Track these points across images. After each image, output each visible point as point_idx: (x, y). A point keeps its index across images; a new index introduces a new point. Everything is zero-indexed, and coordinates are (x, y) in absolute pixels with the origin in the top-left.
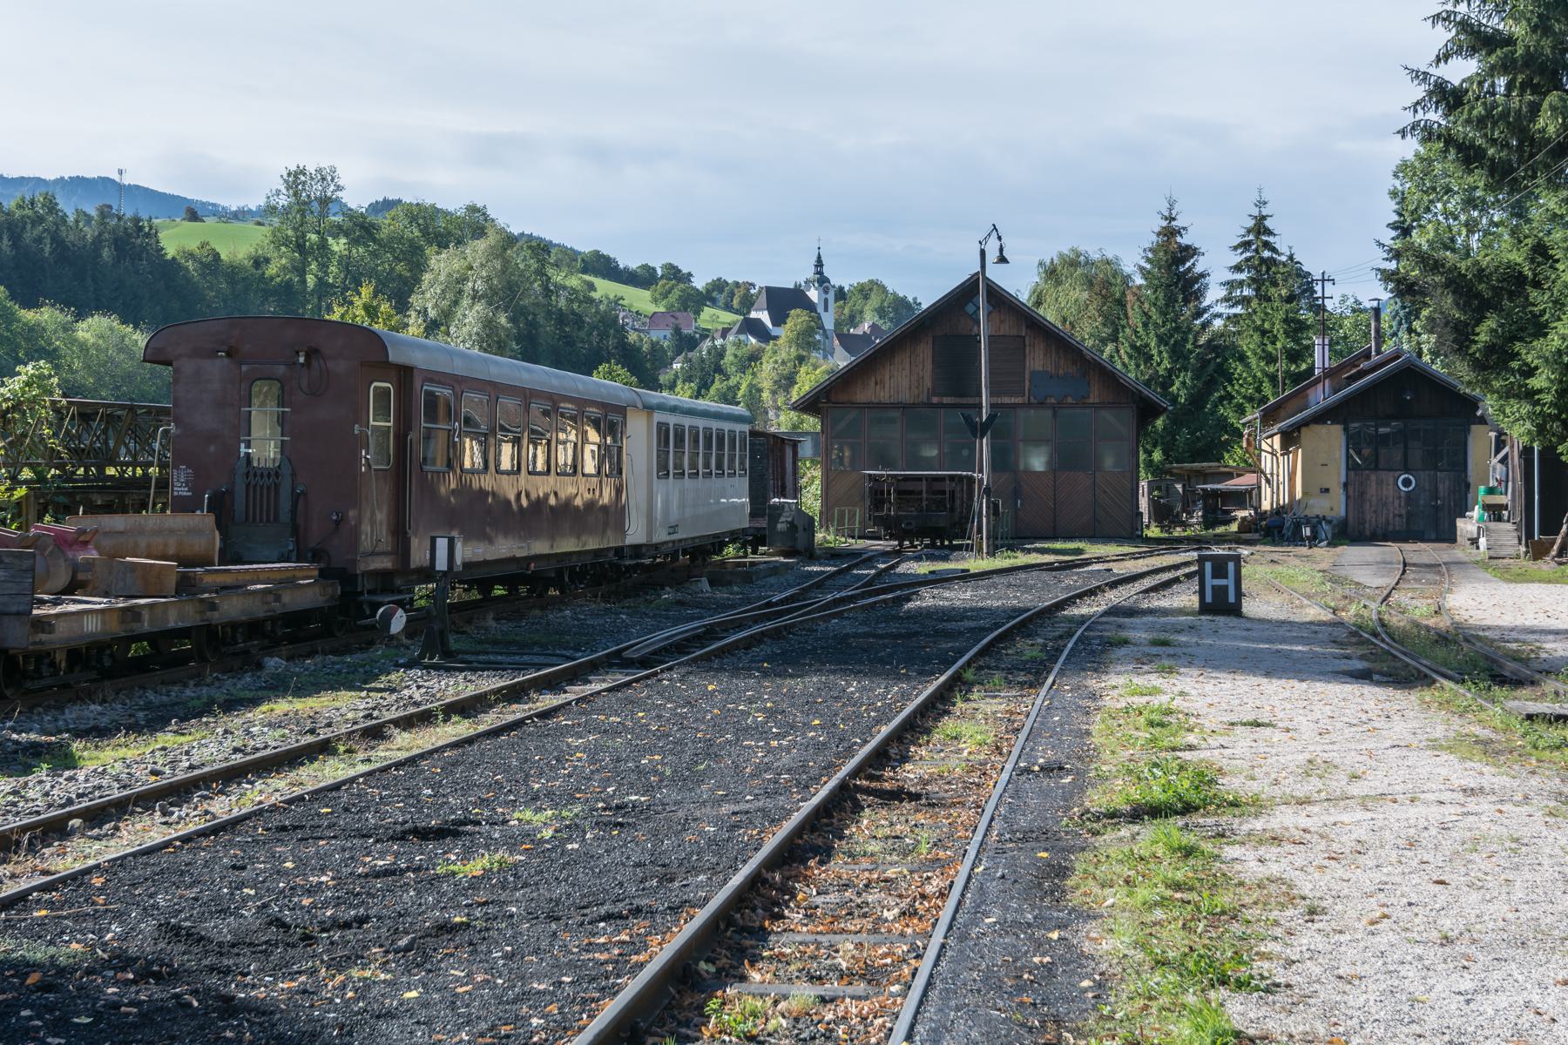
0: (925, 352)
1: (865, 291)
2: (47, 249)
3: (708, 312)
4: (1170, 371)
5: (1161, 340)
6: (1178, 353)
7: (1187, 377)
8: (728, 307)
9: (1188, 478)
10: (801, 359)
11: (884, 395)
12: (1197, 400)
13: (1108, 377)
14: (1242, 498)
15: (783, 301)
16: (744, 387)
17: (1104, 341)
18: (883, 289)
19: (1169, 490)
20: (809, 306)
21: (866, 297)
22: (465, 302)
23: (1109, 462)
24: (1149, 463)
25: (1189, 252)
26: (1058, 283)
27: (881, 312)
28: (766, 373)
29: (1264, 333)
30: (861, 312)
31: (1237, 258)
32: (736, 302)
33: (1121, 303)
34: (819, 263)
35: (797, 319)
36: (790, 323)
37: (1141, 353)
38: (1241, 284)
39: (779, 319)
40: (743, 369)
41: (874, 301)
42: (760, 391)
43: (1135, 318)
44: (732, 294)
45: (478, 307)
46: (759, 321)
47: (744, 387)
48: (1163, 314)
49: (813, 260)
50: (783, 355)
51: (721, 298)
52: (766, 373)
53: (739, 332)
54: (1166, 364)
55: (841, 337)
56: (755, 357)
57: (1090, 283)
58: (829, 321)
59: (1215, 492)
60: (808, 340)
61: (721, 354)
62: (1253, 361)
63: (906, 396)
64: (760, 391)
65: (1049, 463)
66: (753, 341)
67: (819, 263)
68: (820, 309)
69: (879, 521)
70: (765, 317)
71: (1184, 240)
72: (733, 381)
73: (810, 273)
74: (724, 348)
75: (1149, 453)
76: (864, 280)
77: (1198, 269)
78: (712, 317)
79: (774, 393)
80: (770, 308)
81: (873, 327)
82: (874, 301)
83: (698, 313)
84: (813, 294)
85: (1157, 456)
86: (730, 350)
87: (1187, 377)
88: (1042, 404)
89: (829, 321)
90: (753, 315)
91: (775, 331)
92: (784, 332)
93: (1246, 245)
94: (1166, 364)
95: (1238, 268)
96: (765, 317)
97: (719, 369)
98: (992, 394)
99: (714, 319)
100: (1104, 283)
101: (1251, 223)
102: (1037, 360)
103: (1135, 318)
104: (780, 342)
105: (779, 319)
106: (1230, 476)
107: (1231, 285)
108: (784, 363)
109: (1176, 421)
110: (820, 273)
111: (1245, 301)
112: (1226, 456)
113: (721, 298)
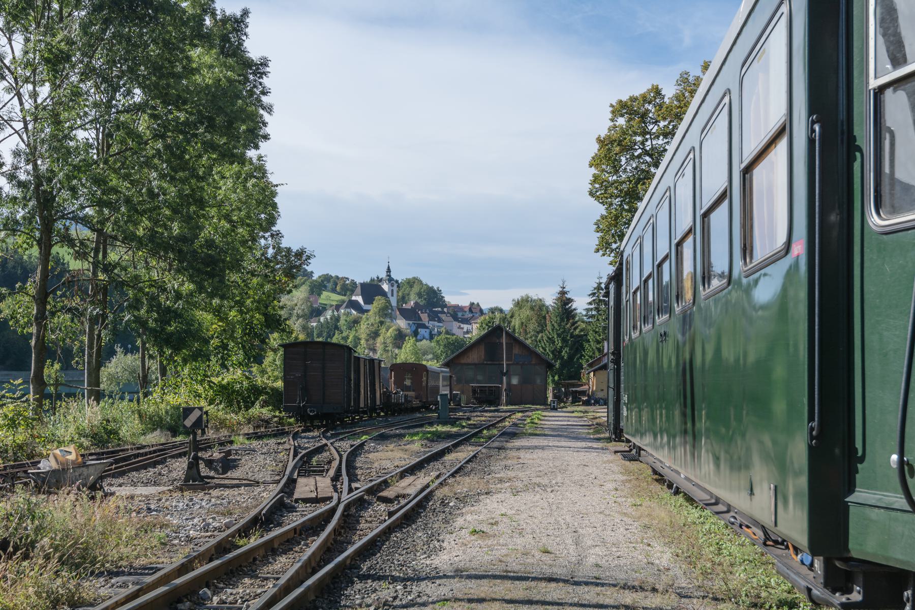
0: (482, 348)
1: (411, 283)
2: (19, 272)
3: (325, 294)
4: (561, 347)
5: (559, 335)
6: (564, 340)
7: (567, 349)
8: (334, 291)
9: (567, 386)
10: (382, 323)
11: (469, 361)
12: (571, 357)
13: (537, 355)
14: (583, 393)
15: (371, 290)
16: (351, 337)
17: (538, 333)
18: (420, 282)
19: (560, 390)
20: (384, 294)
21: (411, 287)
22: (294, 318)
23: (538, 381)
24: (553, 381)
25: (570, 301)
26: (520, 308)
27: (420, 295)
28: (363, 329)
29: (596, 332)
30: (408, 295)
31: (590, 299)
32: (338, 288)
33: (545, 318)
34: (389, 270)
35: (379, 302)
36: (375, 304)
37: (551, 340)
38: (591, 309)
39: (369, 300)
40: (350, 328)
41: (416, 289)
42: (359, 339)
43: (549, 328)
44: (336, 284)
45: (301, 320)
46: (357, 302)
47: (351, 337)
48: (560, 325)
49: (386, 269)
50: (372, 320)
51: (330, 285)
52: (363, 329)
53: (347, 307)
54: (560, 344)
55: (399, 309)
56: (356, 322)
57: (532, 308)
58: (394, 301)
59: (576, 391)
60: (385, 312)
61: (338, 319)
62: (592, 343)
63: (476, 361)
64: (359, 339)
65: (519, 381)
66: (354, 312)
67: (389, 270)
68: (389, 295)
69: (475, 398)
70: (360, 299)
71: (568, 296)
72: (345, 334)
73: (383, 275)
74: (339, 316)
75: (553, 377)
76: (410, 277)
77: (573, 307)
78: (328, 297)
79: (367, 340)
80: (363, 295)
81: (416, 303)
82: (416, 289)
83: (319, 295)
84: (385, 287)
85: (556, 378)
86: (343, 318)
87: (567, 349)
88: (517, 364)
89: (394, 301)
90: (354, 298)
91: (366, 307)
92: (373, 308)
93: (593, 294)
94: (560, 344)
95: (590, 303)
96: (360, 299)
97: (337, 328)
98: (507, 360)
99: (328, 298)
100: (538, 307)
101: (596, 285)
102: (516, 350)
103: (549, 328)
104: (370, 313)
105: (369, 300)
106: (582, 385)
107: (587, 310)
108: (372, 325)
109: (563, 365)
110: (389, 276)
111: (592, 316)
112: (751, 358)
113: (330, 285)
